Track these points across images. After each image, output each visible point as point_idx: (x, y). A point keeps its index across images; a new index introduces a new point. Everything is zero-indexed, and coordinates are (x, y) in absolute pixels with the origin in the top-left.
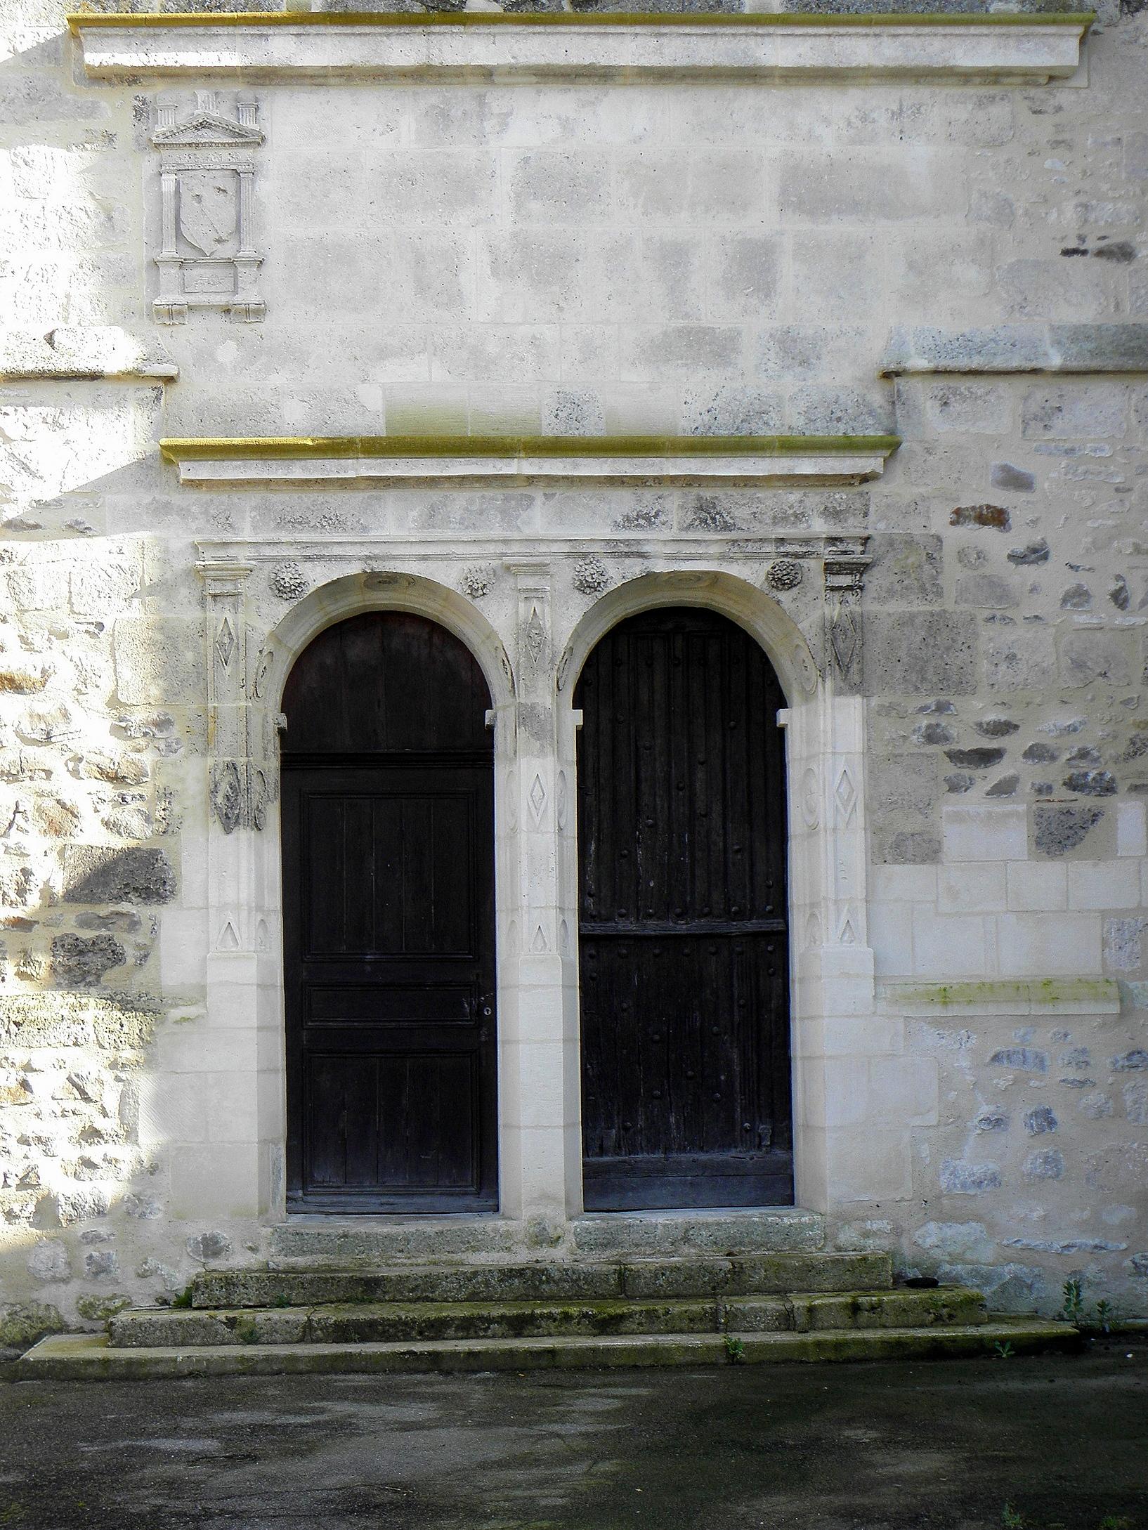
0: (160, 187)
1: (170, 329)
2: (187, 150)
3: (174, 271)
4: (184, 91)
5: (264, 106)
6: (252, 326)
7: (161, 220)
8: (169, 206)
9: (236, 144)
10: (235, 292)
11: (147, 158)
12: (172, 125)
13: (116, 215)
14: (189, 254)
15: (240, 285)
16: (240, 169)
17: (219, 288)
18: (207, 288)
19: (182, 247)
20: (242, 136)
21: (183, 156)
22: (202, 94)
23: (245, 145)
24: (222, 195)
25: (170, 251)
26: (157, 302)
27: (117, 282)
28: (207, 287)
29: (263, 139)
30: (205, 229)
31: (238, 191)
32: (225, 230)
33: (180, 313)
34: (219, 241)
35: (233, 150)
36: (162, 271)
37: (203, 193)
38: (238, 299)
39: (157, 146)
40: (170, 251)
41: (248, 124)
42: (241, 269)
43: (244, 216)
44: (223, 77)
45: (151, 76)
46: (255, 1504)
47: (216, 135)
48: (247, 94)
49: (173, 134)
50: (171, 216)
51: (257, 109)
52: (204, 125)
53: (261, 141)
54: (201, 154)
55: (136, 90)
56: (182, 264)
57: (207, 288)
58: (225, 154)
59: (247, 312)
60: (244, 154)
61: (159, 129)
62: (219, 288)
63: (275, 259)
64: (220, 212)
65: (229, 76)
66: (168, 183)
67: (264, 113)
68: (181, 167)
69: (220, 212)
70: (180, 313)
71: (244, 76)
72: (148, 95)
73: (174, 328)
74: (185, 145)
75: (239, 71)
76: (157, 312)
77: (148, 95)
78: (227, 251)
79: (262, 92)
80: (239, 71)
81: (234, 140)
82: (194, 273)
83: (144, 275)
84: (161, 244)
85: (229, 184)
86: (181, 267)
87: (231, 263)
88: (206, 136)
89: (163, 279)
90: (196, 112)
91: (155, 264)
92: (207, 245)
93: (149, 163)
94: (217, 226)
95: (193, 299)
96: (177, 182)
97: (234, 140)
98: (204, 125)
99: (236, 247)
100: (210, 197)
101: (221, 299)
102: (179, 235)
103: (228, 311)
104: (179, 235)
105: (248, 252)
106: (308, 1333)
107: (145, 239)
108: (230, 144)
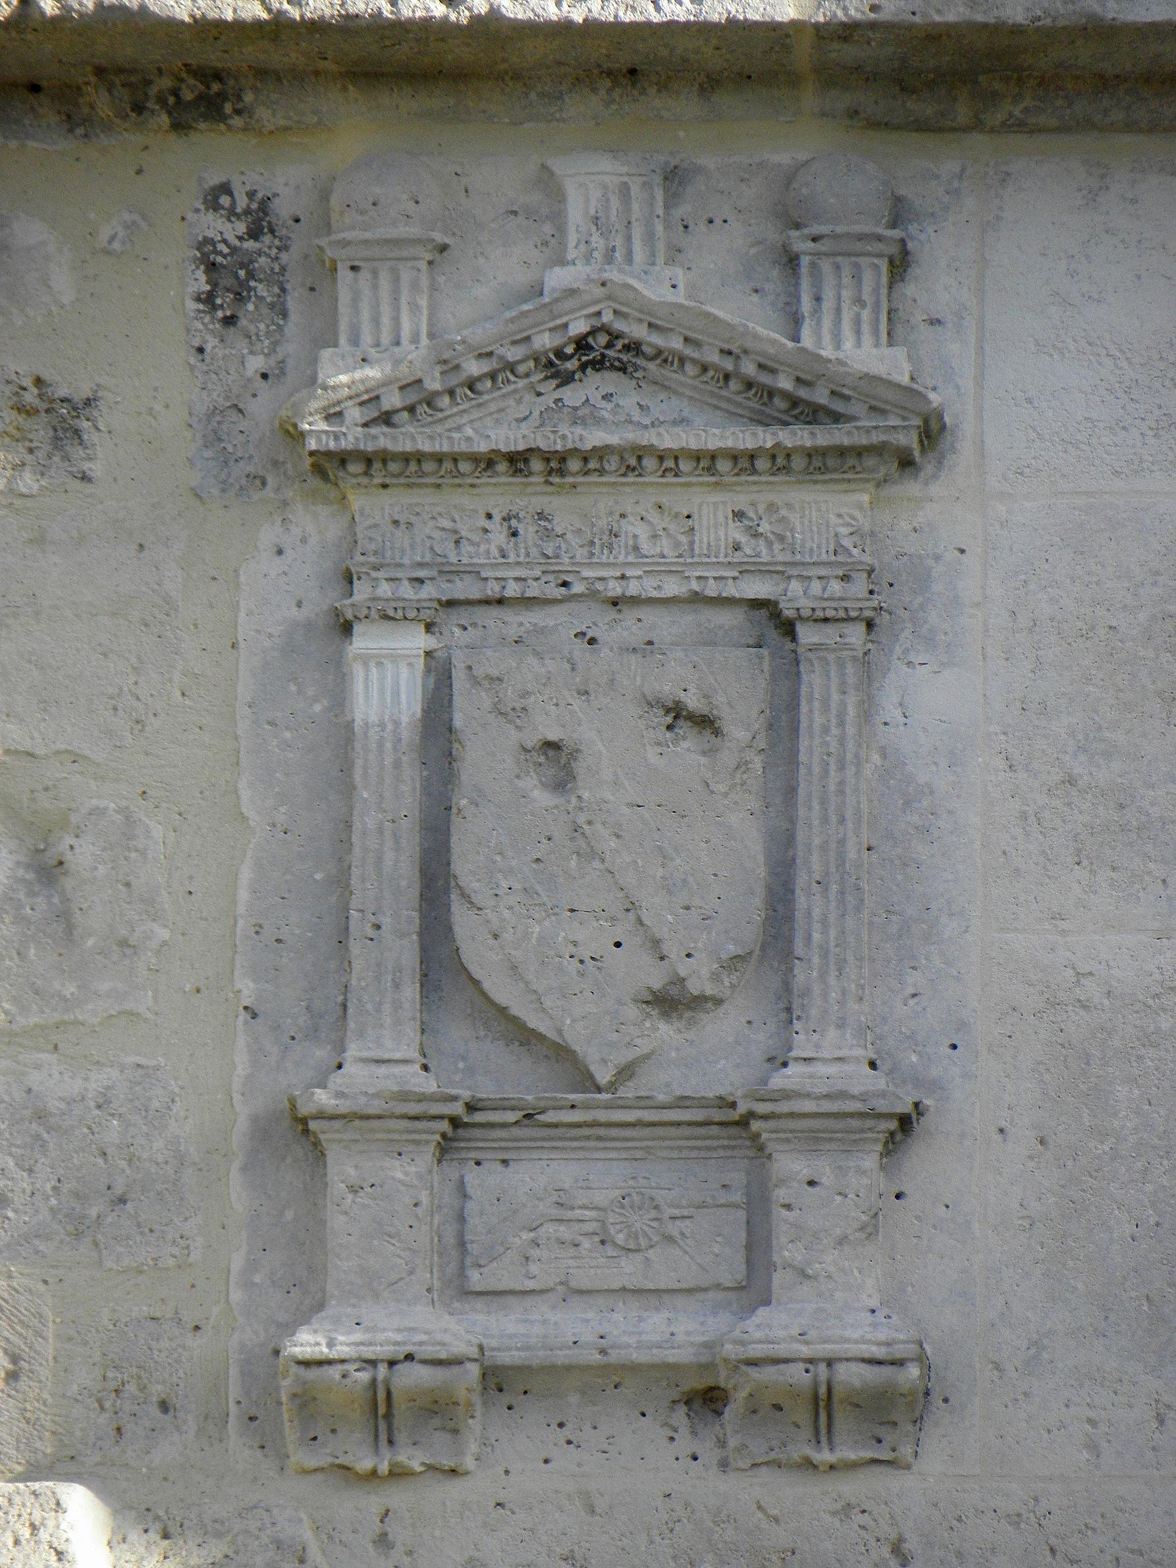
0: (339, 698)
1: (373, 1502)
2: (501, 494)
3: (409, 1172)
4: (491, 169)
5: (941, 250)
6: (851, 1487)
7: (341, 882)
8: (387, 803)
9: (780, 461)
10: (753, 1288)
11: (269, 535)
12: (416, 357)
13: (83, 854)
14: (500, 1075)
15: (787, 1251)
16: (796, 596)
17: (666, 1265)
18: (594, 1268)
19: (458, 1034)
20: (813, 414)
21: (472, 527)
22: (592, 181)
23: (825, 464)
24: (689, 743)
25: (386, 1058)
26: (308, 1342)
27: (79, 1228)
28: (594, 1265)
29: (933, 432)
30: (593, 937)
31: (783, 723)
32: (708, 926)
33: (439, 1410)
34: (670, 1002)
35: (752, 495)
36: (343, 1167)
37: (583, 728)
38: (776, 1328)
39: (329, 466)
40: (386, 1058)
41: (846, 342)
42: (790, 1164)
43: (812, 864)
44: (710, 83)
45: (299, 78)
46: (397, 1137)
47: (664, 407)
48: (845, 176)
49: (420, 402)
50: (401, 864)
51: (900, 264)
52: (598, 353)
53: (914, 443)
54: (574, 511)
55: (217, 155)
56: (459, 1132)
57: (594, 1268)
58: (713, 514)
59: (823, 1406)
60: (823, 515)
61: (342, 377)
62: (666, 1265)
63: (989, 1113)
64: (671, 839)
65: (745, 78)
66: (386, 678)
67: (938, 284)
68: (462, 589)
69: (671, 839)
70: (439, 1410)
71: (832, 77)
72: (286, 181)
73: (398, 1497)
74: (487, 462)
75: (803, 55)
76: (306, 1403)
77: (286, 181)
78: (712, 1058)
79: (932, 171)
80: (803, 55)
81: (766, 438)
82: (526, 1181)
83: (237, 1193)
84: (333, 1020)
85: (735, 685)
86: (446, 1148)
87: (736, 1127)
88: (610, 413)
89: (345, 1219)
90: (557, 279)
91: (299, 1134)
92: (596, 1021)
93: (280, 562)
94: (660, 914)
95: (510, 1332)
96: (439, 673)
97: (766, 438)
98: (598, 353)
99: (762, 1040)
100: (623, 756)
101: (672, 1333)
102: (440, 966)
103: (707, 1400)
104: (440, 966)
105: (830, 1064)
106: (858, 811)
107: (247, 989)
108: (745, 461)
